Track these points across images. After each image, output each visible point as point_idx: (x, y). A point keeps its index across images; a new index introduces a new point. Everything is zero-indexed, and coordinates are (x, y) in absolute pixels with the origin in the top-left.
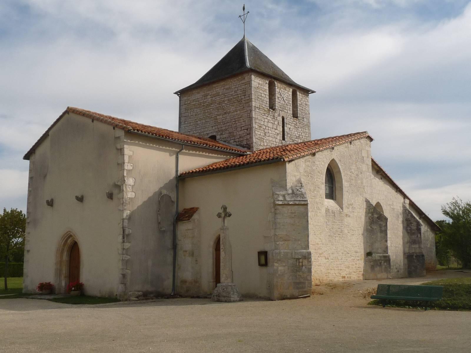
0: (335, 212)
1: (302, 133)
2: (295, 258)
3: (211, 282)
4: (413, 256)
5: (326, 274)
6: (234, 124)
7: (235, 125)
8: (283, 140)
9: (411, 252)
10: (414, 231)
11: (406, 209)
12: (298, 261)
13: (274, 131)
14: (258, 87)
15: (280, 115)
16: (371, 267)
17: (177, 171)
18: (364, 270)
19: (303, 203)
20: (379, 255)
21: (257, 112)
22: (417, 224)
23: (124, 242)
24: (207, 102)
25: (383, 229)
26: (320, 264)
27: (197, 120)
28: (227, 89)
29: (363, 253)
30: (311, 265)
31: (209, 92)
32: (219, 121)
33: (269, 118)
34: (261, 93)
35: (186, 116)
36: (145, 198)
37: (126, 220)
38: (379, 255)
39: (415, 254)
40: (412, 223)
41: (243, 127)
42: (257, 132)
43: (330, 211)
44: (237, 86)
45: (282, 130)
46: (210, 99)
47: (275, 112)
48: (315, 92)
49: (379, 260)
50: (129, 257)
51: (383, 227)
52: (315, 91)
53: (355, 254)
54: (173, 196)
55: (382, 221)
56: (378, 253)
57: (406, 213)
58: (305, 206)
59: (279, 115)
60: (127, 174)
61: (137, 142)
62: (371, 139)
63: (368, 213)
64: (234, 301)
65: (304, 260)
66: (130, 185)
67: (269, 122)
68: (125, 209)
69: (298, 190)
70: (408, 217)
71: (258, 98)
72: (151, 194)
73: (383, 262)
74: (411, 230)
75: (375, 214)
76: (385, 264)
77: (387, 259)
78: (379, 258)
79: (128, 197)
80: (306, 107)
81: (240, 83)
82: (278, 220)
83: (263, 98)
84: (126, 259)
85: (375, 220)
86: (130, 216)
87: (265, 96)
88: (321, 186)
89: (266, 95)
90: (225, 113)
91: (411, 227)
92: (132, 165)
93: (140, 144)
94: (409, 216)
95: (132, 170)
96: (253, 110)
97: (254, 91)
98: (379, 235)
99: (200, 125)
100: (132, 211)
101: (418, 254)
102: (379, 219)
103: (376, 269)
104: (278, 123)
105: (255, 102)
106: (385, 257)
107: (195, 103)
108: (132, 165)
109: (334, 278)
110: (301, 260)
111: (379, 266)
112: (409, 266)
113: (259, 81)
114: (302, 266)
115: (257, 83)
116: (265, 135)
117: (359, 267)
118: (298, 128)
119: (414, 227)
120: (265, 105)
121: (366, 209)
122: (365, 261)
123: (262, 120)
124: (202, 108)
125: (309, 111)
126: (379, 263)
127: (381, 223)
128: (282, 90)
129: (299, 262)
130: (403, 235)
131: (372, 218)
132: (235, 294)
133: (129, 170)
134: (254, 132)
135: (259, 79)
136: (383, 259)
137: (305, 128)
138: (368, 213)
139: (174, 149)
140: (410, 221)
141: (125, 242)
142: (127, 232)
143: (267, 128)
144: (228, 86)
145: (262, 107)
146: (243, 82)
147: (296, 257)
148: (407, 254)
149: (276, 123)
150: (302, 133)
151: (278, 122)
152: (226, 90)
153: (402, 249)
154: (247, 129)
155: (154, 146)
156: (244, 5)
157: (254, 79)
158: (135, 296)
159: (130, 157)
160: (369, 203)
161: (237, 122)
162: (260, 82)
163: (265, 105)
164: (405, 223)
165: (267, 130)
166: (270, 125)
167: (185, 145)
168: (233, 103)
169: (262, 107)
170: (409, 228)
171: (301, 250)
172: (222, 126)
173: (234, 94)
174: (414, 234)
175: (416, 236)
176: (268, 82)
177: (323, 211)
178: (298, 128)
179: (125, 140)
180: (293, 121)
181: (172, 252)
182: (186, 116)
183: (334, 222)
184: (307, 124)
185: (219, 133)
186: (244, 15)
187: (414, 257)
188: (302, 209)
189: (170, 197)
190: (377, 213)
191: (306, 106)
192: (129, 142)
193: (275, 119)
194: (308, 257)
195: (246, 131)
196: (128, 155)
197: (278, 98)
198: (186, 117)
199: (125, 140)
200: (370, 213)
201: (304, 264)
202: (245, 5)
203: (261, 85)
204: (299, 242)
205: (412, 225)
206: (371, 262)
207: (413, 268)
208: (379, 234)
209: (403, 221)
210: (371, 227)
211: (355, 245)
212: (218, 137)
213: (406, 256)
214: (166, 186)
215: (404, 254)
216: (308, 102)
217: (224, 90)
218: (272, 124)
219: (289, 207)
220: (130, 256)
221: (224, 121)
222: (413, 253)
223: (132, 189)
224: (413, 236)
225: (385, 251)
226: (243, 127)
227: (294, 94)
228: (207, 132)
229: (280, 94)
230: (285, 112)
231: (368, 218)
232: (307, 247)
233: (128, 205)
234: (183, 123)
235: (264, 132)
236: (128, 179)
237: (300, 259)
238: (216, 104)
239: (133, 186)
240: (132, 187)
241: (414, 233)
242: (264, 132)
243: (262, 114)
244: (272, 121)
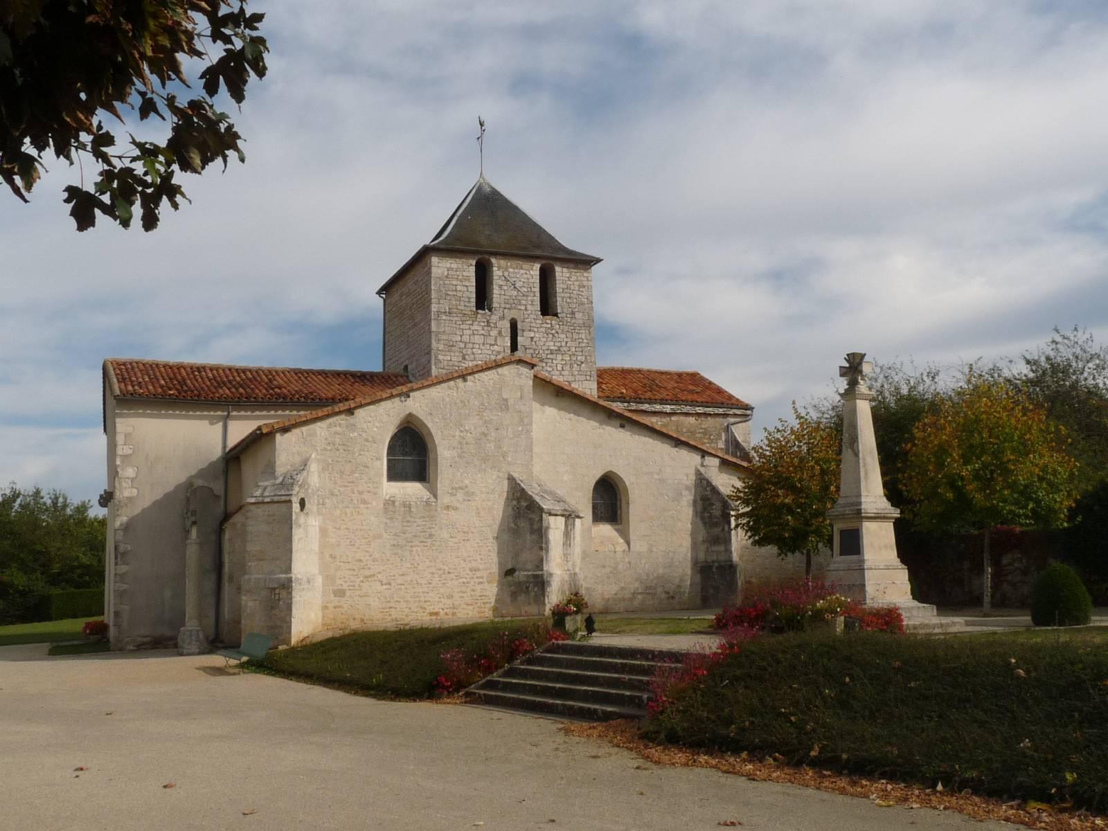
2: (269, 588)
4: (711, 567)
9: (709, 561)
10: (716, 520)
11: (702, 477)
13: (488, 348)
14: (448, 274)
15: (504, 318)
16: (512, 596)
17: (224, 447)
18: (496, 600)
19: (283, 498)
20: (525, 573)
21: (442, 321)
22: (723, 506)
25: (536, 527)
29: (497, 571)
30: (291, 599)
33: (474, 327)
34: (456, 285)
36: (158, 494)
37: (120, 531)
38: (525, 573)
39: (716, 564)
40: (713, 504)
42: (441, 357)
43: (397, 504)
45: (509, 344)
47: (492, 314)
49: (526, 582)
50: (126, 586)
51: (536, 524)
52: (597, 256)
53: (470, 573)
54: (218, 487)
55: (533, 512)
56: (526, 570)
57: (702, 486)
58: (289, 504)
59: (502, 318)
60: (123, 462)
61: (141, 411)
63: (512, 500)
64: (192, 654)
65: (281, 591)
66: (128, 478)
67: (474, 334)
68: (118, 515)
70: (706, 493)
71: (447, 294)
72: (170, 488)
73: (531, 585)
74: (710, 517)
75: (522, 500)
76: (536, 589)
77: (540, 579)
78: (525, 579)
79: (125, 495)
80: (582, 292)
84: (122, 589)
85: (522, 512)
86: (127, 524)
88: (373, 464)
89: (467, 286)
91: (711, 511)
92: (132, 447)
93: (148, 413)
94: (707, 491)
95: (131, 455)
96: (433, 318)
97: (436, 283)
98: (528, 538)
100: (130, 516)
101: (722, 564)
102: (528, 510)
103: (519, 598)
104: (500, 333)
106: (535, 576)
108: (132, 447)
109: (404, 617)
110: (277, 591)
111: (525, 593)
112: (704, 588)
113: (451, 263)
114: (279, 600)
115: (446, 269)
117: (480, 596)
118: (556, 335)
119: (716, 511)
120: (465, 306)
121: (508, 492)
122: (501, 585)
123: (456, 334)
125: (590, 298)
126: (524, 588)
127: (533, 516)
129: (275, 594)
130: (692, 528)
131: (518, 508)
132: (194, 643)
133: (126, 456)
134: (433, 357)
135: (451, 261)
136: (532, 580)
138: (512, 500)
139: (219, 413)
140: (708, 499)
141: (119, 563)
142: (122, 549)
143: (471, 345)
145: (457, 309)
147: (271, 586)
148: (699, 565)
149: (494, 333)
153: (689, 555)
155: (177, 412)
157: (438, 263)
158: (136, 644)
159: (127, 436)
160: (514, 482)
163: (465, 306)
164: (700, 503)
166: (478, 339)
167: (232, 405)
169: (457, 309)
170: (706, 515)
171: (279, 574)
174: (716, 525)
175: (720, 529)
176: (474, 262)
177: (378, 505)
178: (556, 335)
179: (117, 411)
180: (543, 323)
181: (213, 577)
183: (408, 521)
184: (584, 324)
187: (714, 570)
188: (283, 507)
189: (211, 489)
190: (526, 500)
191: (581, 289)
192: (125, 413)
193: (490, 326)
194: (287, 586)
197: (500, 286)
199: (117, 411)
200: (515, 500)
203: (456, 271)
204: (278, 563)
205: (714, 507)
206: (510, 587)
207: (711, 591)
208: (528, 537)
209: (695, 502)
210: (515, 525)
213: (698, 569)
214: (202, 474)
215: (695, 562)
216: (588, 280)
218: (482, 336)
219: (266, 506)
220: (128, 584)
222: (713, 562)
223: (132, 484)
224: (715, 529)
225: (538, 567)
229: (504, 279)
230: (520, 309)
231: (510, 509)
232: (288, 569)
233: (124, 509)
235: (461, 354)
236: (123, 470)
237: (276, 588)
239: (133, 480)
240: (132, 481)
241: (716, 522)
242: (461, 354)
243: (456, 323)
244: (483, 332)
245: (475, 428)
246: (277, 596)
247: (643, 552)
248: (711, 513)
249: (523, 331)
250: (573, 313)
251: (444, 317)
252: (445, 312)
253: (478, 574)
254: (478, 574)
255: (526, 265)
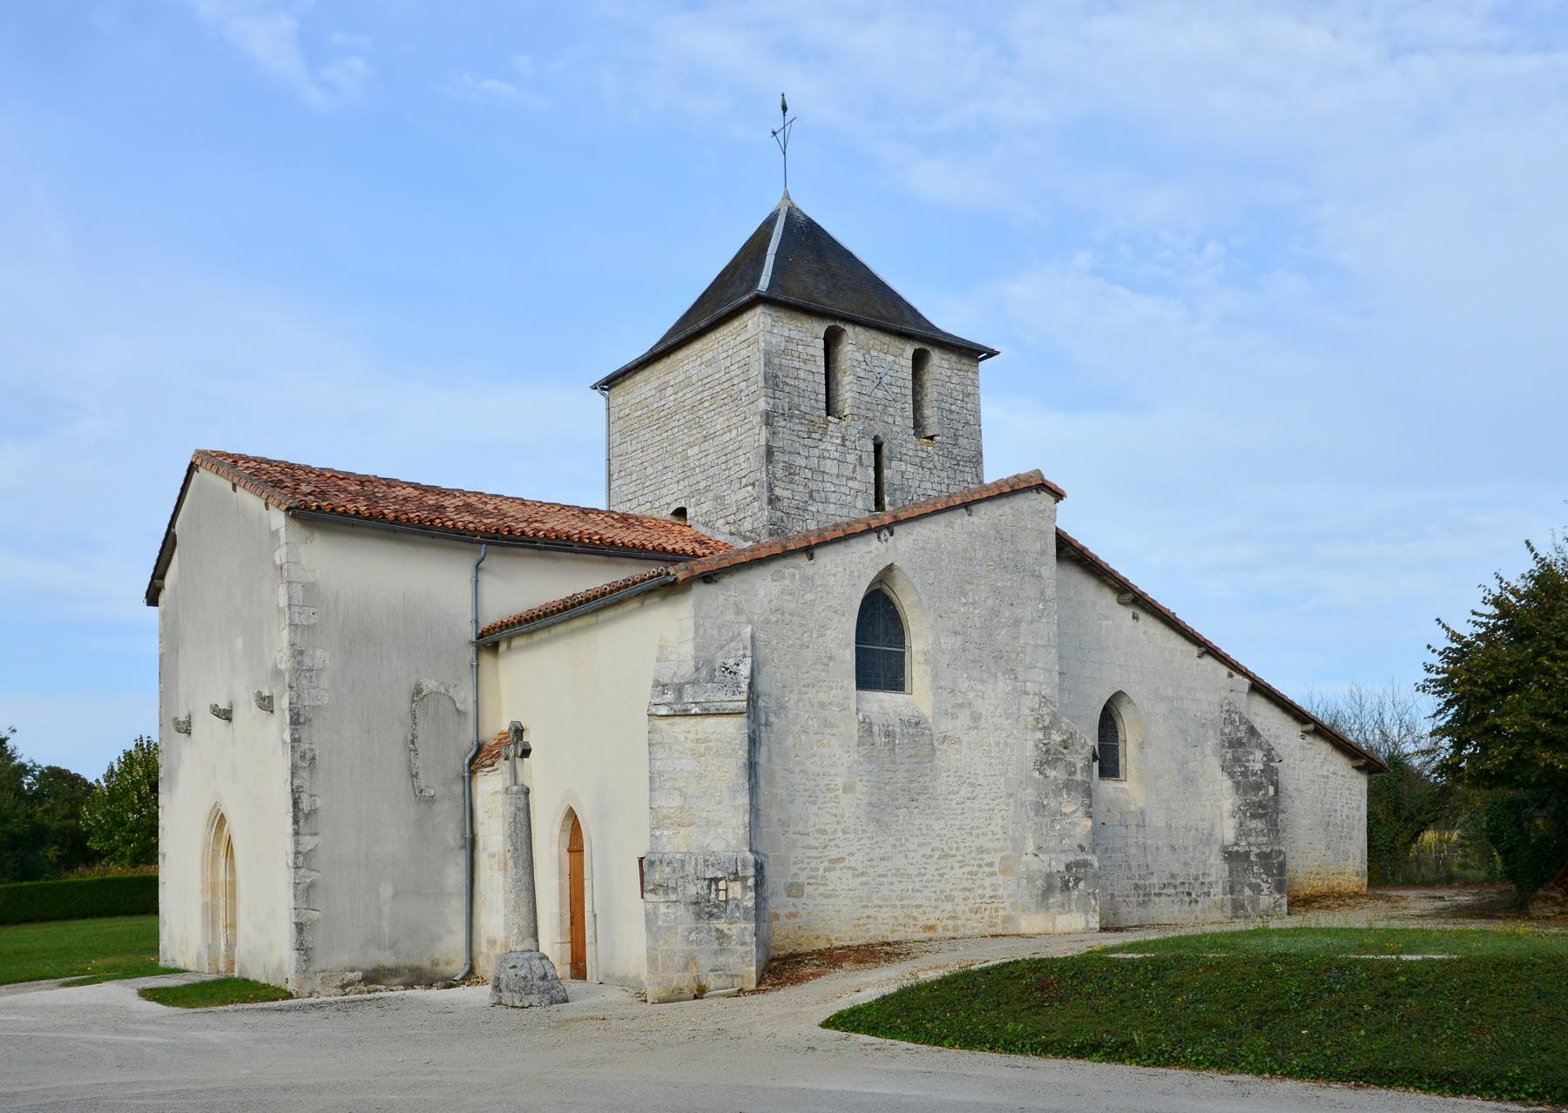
0: (894, 732)
1: (948, 485)
3: (556, 943)
5: (856, 922)
6: (725, 470)
7: (727, 472)
8: (877, 510)
12: (713, 887)
23: (296, 833)
24: (666, 407)
26: (834, 890)
27: (646, 464)
28: (709, 363)
31: (670, 377)
32: (692, 465)
35: (622, 455)
41: (744, 477)
43: (875, 729)
44: (730, 352)
46: (672, 398)
48: (998, 353)
62: (1058, 495)
65: (731, 885)
69: (727, 669)
70: (1239, 735)
74: (1244, 774)
81: (737, 341)
82: (659, 763)
83: (802, 385)
87: (810, 377)
89: (813, 373)
90: (705, 437)
91: (1247, 764)
99: (651, 478)
105: (774, 398)
107: (639, 413)
110: (722, 885)
116: (811, 497)
117: (991, 897)
123: (799, 454)
124: (656, 427)
128: (874, 353)
129: (718, 890)
137: (960, 468)
144: (709, 356)
146: (742, 338)
149: (851, 458)
150: (948, 485)
151: (860, 457)
152: (706, 367)
154: (753, 484)
156: (783, 95)
161: (731, 463)
162: (794, 334)
165: (820, 483)
168: (721, 407)
172: (700, 477)
173: (724, 379)
182: (622, 455)
185: (693, 500)
186: (784, 128)
195: (750, 488)
196: (301, 583)
198: (622, 458)
200: (1040, 729)
201: (730, 896)
202: (785, 97)
211: (980, 831)
212: (690, 512)
217: (703, 366)
219: (693, 721)
221: (703, 461)
226: (744, 477)
227: (919, 360)
228: (668, 499)
230: (887, 423)
234: (615, 477)
237: (721, 879)
238: (685, 414)
244: (836, 455)
245: (997, 599)
246: (722, 894)
247: (1160, 827)
248: (1246, 767)
249: (891, 460)
250: (956, 437)
251: (782, 423)
252: (783, 414)
253: (988, 858)
254: (988, 858)
255: (895, 344)
